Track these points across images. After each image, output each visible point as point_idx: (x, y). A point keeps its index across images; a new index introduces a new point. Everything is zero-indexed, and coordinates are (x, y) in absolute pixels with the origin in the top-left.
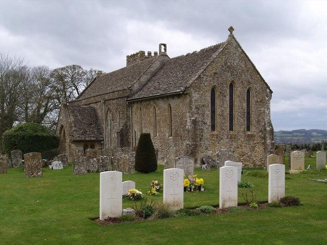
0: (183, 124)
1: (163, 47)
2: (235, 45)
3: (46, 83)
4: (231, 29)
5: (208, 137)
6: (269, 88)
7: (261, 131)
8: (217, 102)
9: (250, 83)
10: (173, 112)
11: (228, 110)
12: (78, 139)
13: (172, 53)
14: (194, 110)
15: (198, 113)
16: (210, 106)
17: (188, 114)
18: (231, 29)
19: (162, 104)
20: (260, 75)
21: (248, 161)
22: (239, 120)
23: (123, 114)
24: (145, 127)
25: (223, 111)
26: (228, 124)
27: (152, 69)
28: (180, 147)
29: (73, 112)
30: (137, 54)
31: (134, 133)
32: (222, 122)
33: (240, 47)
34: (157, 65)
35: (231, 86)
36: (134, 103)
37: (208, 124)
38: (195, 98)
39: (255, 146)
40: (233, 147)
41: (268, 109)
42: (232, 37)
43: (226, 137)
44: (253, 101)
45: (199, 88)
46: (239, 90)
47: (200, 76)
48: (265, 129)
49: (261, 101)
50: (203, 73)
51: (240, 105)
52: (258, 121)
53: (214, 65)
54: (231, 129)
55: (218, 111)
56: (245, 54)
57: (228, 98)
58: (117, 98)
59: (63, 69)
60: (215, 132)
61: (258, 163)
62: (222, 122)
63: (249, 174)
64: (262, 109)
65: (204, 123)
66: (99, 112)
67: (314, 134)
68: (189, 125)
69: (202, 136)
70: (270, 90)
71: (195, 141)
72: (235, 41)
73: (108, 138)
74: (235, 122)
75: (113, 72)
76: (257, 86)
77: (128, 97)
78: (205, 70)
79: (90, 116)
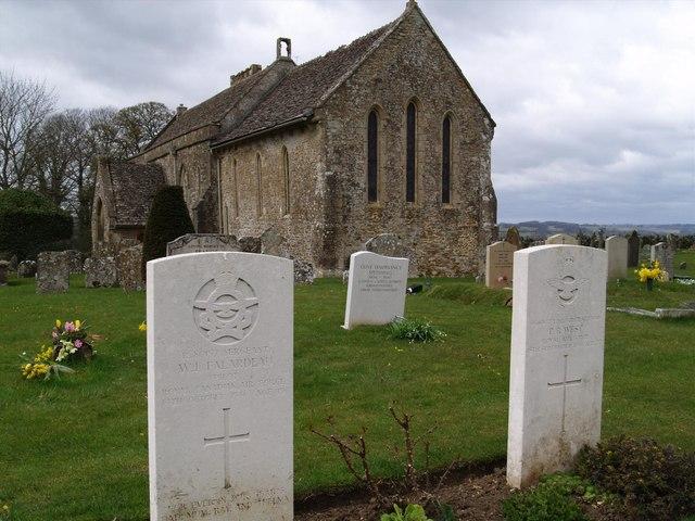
0: (309, 186)
1: (284, 44)
2: (419, 23)
3: (109, 134)
5: (363, 213)
6: (488, 115)
7: (471, 204)
8: (382, 140)
9: (449, 103)
10: (292, 162)
12: (125, 223)
13: (302, 55)
14: (332, 156)
15: (340, 163)
17: (319, 165)
19: (273, 150)
20: (471, 90)
21: (445, 264)
22: (428, 182)
23: (205, 173)
24: (243, 197)
25: (392, 160)
26: (403, 188)
27: (262, 87)
29: (119, 173)
30: (248, 70)
31: (224, 210)
33: (431, 29)
34: (274, 77)
35: (412, 109)
37: (362, 185)
38: (334, 131)
39: (460, 233)
40: (413, 234)
41: (487, 158)
43: (399, 214)
44: (455, 141)
45: (343, 110)
46: (425, 117)
47: (344, 84)
48: (480, 200)
49: (473, 142)
50: (351, 77)
52: (467, 184)
53: (375, 63)
54: (410, 197)
55: (383, 159)
57: (403, 133)
58: (195, 144)
59: (134, 109)
60: (377, 204)
61: (464, 268)
63: (440, 291)
64: (475, 158)
65: (354, 184)
66: (168, 172)
68: (320, 189)
69: (349, 210)
70: (491, 121)
71: (333, 221)
72: (421, 14)
74: (419, 182)
76: (465, 111)
77: (212, 140)
78: (356, 71)
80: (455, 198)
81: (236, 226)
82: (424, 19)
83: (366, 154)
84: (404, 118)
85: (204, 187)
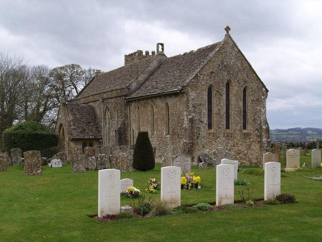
0: (180, 122)
1: (160, 46)
2: (231, 44)
3: (46, 82)
4: (228, 29)
5: (205, 135)
6: (265, 87)
7: (257, 130)
8: (214, 100)
9: (246, 82)
10: (170, 110)
11: (225, 108)
12: (76, 137)
13: (170, 53)
14: (191, 108)
15: (195, 112)
16: (207, 105)
17: (185, 113)
18: (228, 29)
19: (160, 103)
20: (256, 74)
21: (245, 159)
22: (236, 119)
23: (121, 112)
24: (143, 125)
25: (219, 110)
26: (224, 123)
27: (150, 68)
28: (178, 145)
29: (72, 111)
30: (135, 53)
31: (132, 131)
32: (219, 120)
33: (237, 47)
34: (154, 64)
35: (228, 85)
36: (132, 101)
37: (205, 122)
38: (192, 97)
39: (251, 144)
40: (229, 145)
41: (264, 107)
42: (228, 36)
43: (222, 135)
44: (249, 99)
45: (196, 87)
46: (235, 89)
47: (197, 75)
48: (261, 128)
49: (257, 100)
50: (200, 72)
51: (236, 103)
52: (254, 120)
53: (211, 64)
54: (228, 127)
55: (215, 110)
56: (241, 53)
57: (224, 97)
58: (115, 97)
59: (62, 68)
60: (212, 131)
61: (254, 161)
62: (219, 120)
63: (246, 172)
64: (258, 108)
65: (201, 122)
66: (97, 110)
67: (310, 132)
68: (186, 124)
69: (199, 134)
70: (266, 89)
71: (192, 139)
72: (232, 40)
73: (107, 136)
74: (232, 120)
75: (111, 71)
76: (253, 85)
77: (126, 96)
78: (202, 69)
79: (89, 115)
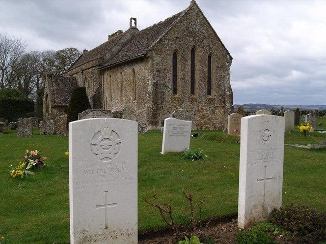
0: (145, 87)
1: (133, 21)
2: (197, 11)
3: (51, 63)
5: (170, 100)
6: (229, 54)
7: (221, 95)
8: (179, 66)
9: (211, 48)
10: (137, 76)
12: (59, 105)
13: (142, 26)
14: (156, 73)
15: (159, 76)
17: (150, 77)
19: (128, 70)
20: (221, 42)
21: (209, 124)
22: (201, 85)
23: (96, 81)
24: (114, 92)
25: (184, 75)
26: (189, 88)
27: (123, 41)
29: (56, 81)
30: (116, 33)
31: (105, 98)
33: (202, 14)
34: (128, 36)
35: (193, 51)
37: (170, 87)
38: (157, 61)
39: (216, 109)
40: (194, 110)
41: (229, 74)
43: (187, 100)
44: (214, 66)
45: (161, 52)
46: (199, 55)
47: (161, 39)
48: (225, 94)
49: (222, 67)
50: (164, 36)
52: (219, 86)
53: (176, 29)
54: (192, 92)
55: (180, 75)
57: (189, 62)
58: (92, 67)
59: (63, 51)
60: (177, 96)
61: (218, 126)
63: (206, 136)
64: (223, 74)
65: (166, 86)
66: (79, 81)
68: (150, 88)
69: (164, 99)
70: (230, 56)
71: (156, 104)
72: (197, 7)
74: (197, 85)
76: (218, 52)
77: (99, 65)
78: (167, 33)
80: (213, 93)
81: (111, 106)
82: (199, 9)
83: (172, 72)
84: (190, 55)
85: (96, 88)
